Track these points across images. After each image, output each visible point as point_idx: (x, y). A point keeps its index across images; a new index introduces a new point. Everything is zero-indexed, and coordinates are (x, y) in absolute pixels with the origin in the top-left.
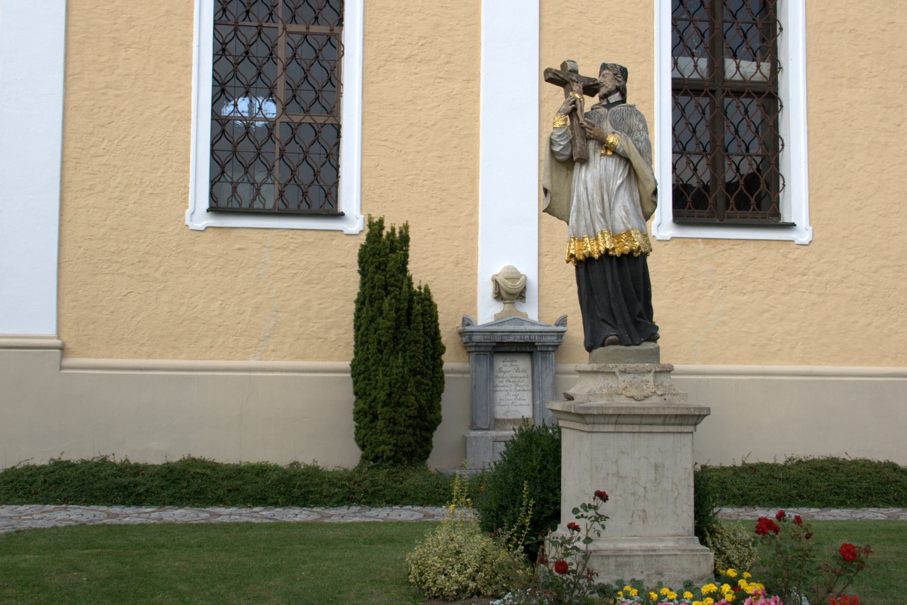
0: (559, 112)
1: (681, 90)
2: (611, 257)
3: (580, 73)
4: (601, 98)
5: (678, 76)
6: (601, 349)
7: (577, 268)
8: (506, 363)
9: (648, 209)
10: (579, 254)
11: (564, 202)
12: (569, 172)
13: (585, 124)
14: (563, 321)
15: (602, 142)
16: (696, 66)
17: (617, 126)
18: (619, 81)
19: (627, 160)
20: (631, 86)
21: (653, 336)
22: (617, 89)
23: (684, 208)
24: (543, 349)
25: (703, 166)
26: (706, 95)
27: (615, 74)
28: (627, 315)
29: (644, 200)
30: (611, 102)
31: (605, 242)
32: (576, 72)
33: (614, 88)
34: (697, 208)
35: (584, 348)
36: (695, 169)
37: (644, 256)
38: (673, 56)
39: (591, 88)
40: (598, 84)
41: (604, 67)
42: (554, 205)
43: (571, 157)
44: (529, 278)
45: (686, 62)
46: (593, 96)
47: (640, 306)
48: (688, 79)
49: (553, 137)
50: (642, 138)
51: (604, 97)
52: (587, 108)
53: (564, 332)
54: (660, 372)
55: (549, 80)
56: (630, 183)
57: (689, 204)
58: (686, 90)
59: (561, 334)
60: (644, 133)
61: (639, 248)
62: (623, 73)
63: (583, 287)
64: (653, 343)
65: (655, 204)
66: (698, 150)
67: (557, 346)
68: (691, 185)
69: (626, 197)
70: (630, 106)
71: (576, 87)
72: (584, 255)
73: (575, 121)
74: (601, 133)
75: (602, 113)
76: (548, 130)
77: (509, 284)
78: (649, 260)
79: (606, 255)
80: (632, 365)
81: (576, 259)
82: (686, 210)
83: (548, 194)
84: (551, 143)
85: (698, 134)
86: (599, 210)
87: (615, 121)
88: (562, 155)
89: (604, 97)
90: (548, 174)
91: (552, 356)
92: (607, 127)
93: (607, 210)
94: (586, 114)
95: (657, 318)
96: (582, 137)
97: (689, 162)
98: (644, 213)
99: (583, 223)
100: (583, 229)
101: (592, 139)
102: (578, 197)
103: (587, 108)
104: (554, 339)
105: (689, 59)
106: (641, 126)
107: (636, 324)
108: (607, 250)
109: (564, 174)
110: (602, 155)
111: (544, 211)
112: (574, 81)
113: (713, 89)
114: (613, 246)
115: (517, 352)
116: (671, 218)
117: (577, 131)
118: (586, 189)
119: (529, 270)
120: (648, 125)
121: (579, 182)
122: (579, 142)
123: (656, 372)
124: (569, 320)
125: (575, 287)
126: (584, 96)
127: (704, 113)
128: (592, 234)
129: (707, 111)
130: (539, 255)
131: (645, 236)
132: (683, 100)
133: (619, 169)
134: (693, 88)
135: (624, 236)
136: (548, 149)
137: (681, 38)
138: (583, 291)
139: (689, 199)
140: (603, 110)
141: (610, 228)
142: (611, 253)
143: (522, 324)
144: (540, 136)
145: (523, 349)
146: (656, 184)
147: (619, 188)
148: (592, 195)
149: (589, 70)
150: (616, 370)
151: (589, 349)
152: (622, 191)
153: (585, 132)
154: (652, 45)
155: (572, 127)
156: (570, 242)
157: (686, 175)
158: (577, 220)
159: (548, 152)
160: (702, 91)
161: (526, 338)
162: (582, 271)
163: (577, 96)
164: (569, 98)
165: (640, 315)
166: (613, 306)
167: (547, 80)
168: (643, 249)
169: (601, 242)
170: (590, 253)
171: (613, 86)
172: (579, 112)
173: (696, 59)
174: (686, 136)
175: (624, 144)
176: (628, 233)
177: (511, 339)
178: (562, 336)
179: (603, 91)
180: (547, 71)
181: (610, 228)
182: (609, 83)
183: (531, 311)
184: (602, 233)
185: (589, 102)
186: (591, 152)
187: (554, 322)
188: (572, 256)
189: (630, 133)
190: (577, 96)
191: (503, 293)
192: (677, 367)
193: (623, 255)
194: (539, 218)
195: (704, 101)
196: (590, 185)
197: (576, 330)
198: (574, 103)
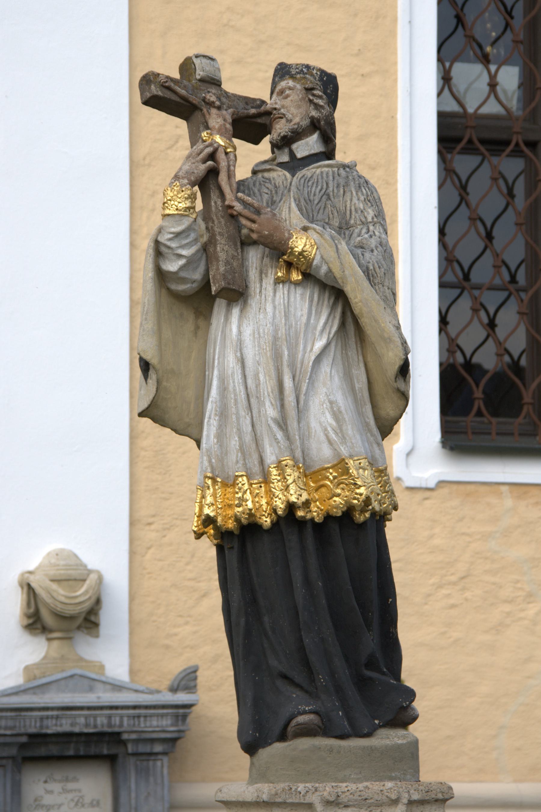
0: (176, 177)
1: (458, 140)
2: (302, 523)
3: (223, 86)
4: (276, 146)
5: (452, 107)
6: (278, 746)
7: (220, 549)
8: (51, 786)
9: (388, 409)
10: (226, 518)
11: (190, 394)
12: (201, 322)
13: (238, 207)
14: (188, 680)
15: (278, 251)
16: (493, 85)
17: (313, 213)
18: (317, 107)
19: (337, 294)
20: (347, 117)
21: (399, 710)
22: (314, 125)
23: (466, 413)
24: (142, 748)
25: (509, 319)
26: (517, 152)
27: (309, 90)
28: (339, 663)
29: (379, 388)
30: (299, 155)
31: (287, 488)
32: (216, 83)
33: (305, 123)
34: (495, 413)
35: (237, 745)
36: (492, 325)
37: (380, 519)
38: (440, 60)
39: (251, 124)
40: (268, 113)
41: (283, 71)
42: (165, 401)
43: (206, 285)
44: (109, 577)
45: (471, 75)
46: (256, 142)
47: (370, 642)
48: (476, 116)
49: (164, 238)
50: (373, 242)
51: (284, 143)
52: (242, 172)
53: (189, 706)
54: (422, 802)
55: (152, 102)
56: (345, 347)
57: (479, 404)
58: (470, 141)
59: (182, 712)
60: (378, 230)
61: (367, 501)
62: (327, 86)
63: (236, 595)
64: (401, 732)
65: (404, 397)
66: (497, 281)
67: (174, 740)
68: (479, 367)
69: (336, 379)
70: (344, 166)
71: (215, 119)
72: (237, 520)
73: (214, 196)
74: (277, 228)
75: (279, 181)
76: (151, 224)
77: (61, 592)
78: (392, 531)
79: (290, 516)
80: (353, 787)
81: (217, 528)
82: (471, 417)
83: (152, 373)
84: (159, 251)
85: (498, 243)
86: (271, 411)
87: (308, 201)
88: (184, 280)
89: (284, 143)
90: (150, 325)
91: (162, 765)
92: (290, 214)
93: (292, 413)
94: (241, 183)
95: (409, 676)
96: (231, 239)
97: (478, 307)
98: (377, 418)
99: (234, 443)
100: (233, 456)
101: (255, 243)
102: (222, 380)
103: (242, 172)
104: (166, 722)
105: (478, 68)
106: (370, 214)
107: (362, 683)
108: (291, 507)
109: (190, 326)
110: (278, 281)
111: (141, 415)
112: (211, 104)
113: (532, 137)
114: (305, 496)
115: (78, 758)
116: (436, 435)
117: (220, 225)
118: (242, 362)
119: (107, 558)
120: (386, 209)
121: (224, 346)
122: (223, 249)
123: (411, 803)
124: (202, 677)
125: (216, 598)
126: (236, 141)
127: (511, 194)
128: (256, 469)
129: (520, 189)
130: (132, 523)
131: (381, 472)
132: (464, 164)
133: (318, 314)
134: (486, 135)
135: (332, 474)
136: (150, 266)
137: (460, 20)
138: (235, 605)
139: (478, 394)
140: (280, 176)
141: (298, 454)
142: (300, 513)
143: (91, 689)
144: (133, 245)
145: (93, 750)
146: (406, 351)
147: (319, 359)
148: (256, 376)
149: (248, 80)
150: (315, 799)
151: (251, 747)
152: (326, 367)
153: (239, 228)
154: (393, 34)
155: (206, 215)
156: (204, 488)
157: (471, 338)
158: (220, 436)
159: (151, 274)
160: (507, 143)
161: (101, 723)
162: (233, 557)
163: (219, 140)
164: (200, 146)
165: (371, 664)
166: (306, 641)
167: (147, 102)
168: (375, 505)
169: (277, 486)
170: (251, 514)
171: (304, 117)
172: (223, 178)
173: (493, 68)
174: (469, 248)
175: (330, 254)
176: (341, 466)
177: (65, 726)
178: (185, 717)
179: (281, 128)
180: (147, 80)
181: (298, 454)
182: (294, 111)
183: (112, 657)
184: (280, 466)
185: (249, 156)
186: (253, 274)
187: (166, 683)
188: (209, 521)
189: (344, 228)
190: (219, 140)
191: (45, 615)
192: (460, 789)
193: (328, 517)
194: (133, 437)
195: (511, 167)
196: (250, 353)
197: (219, 701)
198: (212, 156)
